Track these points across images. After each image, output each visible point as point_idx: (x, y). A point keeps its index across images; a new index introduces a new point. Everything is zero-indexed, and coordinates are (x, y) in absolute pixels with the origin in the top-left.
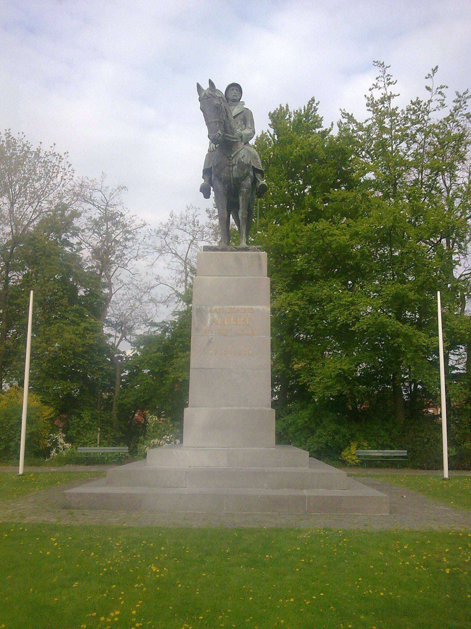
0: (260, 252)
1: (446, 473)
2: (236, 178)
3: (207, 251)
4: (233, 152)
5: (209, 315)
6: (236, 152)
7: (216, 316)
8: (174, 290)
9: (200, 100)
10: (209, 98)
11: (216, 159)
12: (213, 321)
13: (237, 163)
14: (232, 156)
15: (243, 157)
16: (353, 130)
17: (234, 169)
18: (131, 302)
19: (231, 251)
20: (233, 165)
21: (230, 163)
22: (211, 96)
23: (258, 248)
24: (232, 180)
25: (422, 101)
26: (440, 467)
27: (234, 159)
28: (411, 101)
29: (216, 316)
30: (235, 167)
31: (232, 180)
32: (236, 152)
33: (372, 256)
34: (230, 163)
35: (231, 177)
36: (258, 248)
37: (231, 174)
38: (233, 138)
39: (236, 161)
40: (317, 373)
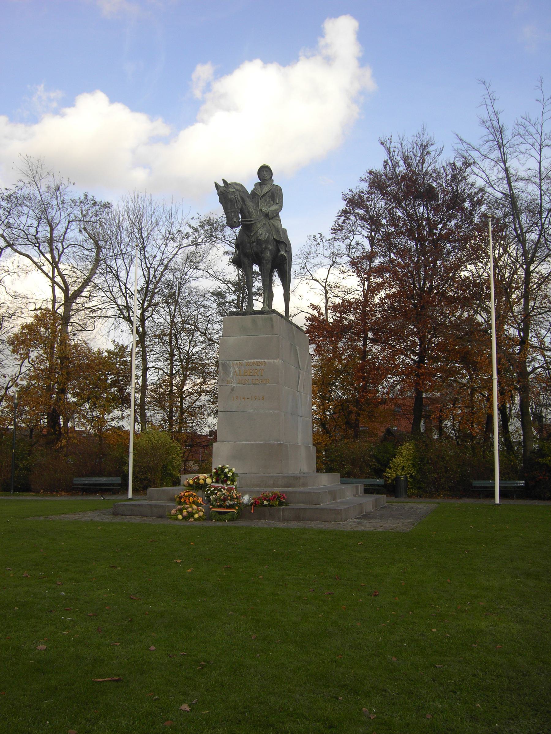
1: (498, 500)
4: (252, 232)
5: (232, 369)
6: (255, 231)
7: (237, 369)
8: (509, 184)
9: (218, 194)
12: (235, 372)
14: (252, 235)
15: (260, 235)
18: (160, 373)
19: (92, 476)
21: (250, 241)
24: (254, 254)
26: (493, 496)
27: (253, 237)
29: (237, 369)
31: (254, 254)
32: (255, 231)
33: (369, 309)
34: (250, 241)
38: (251, 221)
40: (423, 469)
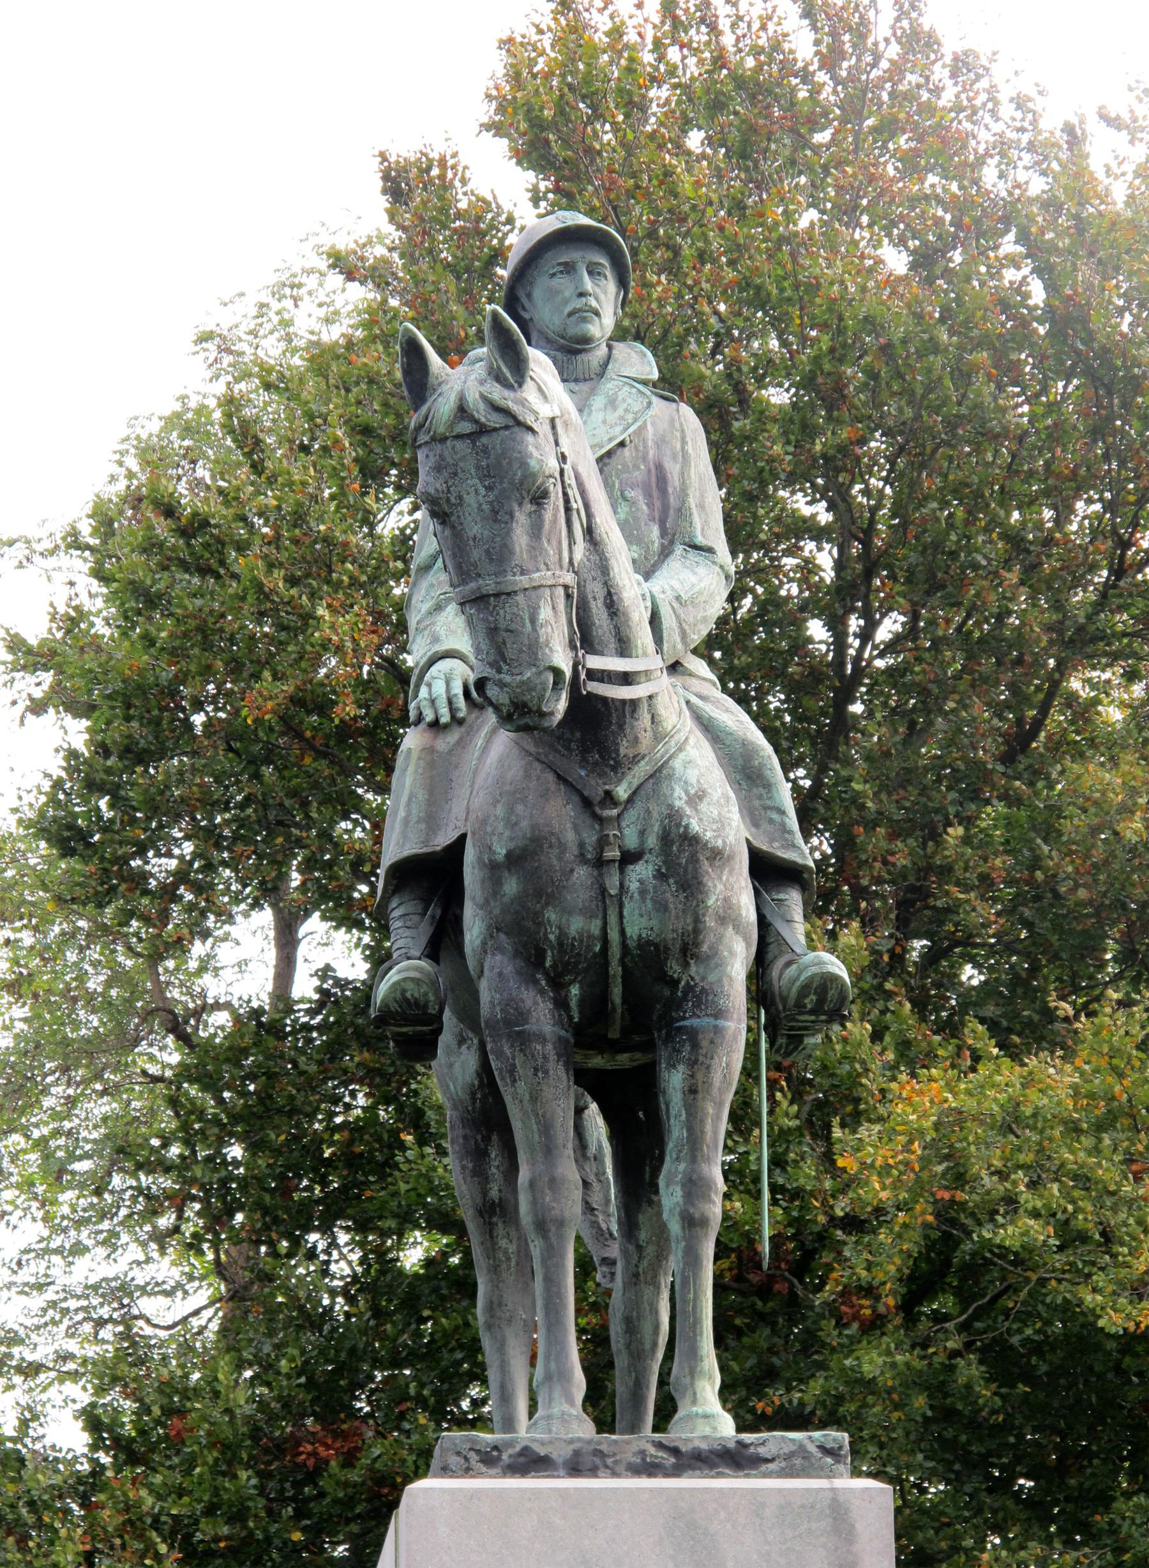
0: (839, 1483)
2: (644, 944)
3: (468, 1472)
10: (483, 430)
11: (500, 810)
13: (652, 841)
16: (269, 1166)
17: (634, 886)
20: (629, 858)
22: (496, 420)
23: (822, 1448)
24: (615, 951)
25: (296, 306)
27: (631, 816)
28: (16, 644)
30: (642, 872)
31: (615, 951)
35: (614, 936)
36: (822, 1448)
37: (613, 919)
39: (642, 833)
